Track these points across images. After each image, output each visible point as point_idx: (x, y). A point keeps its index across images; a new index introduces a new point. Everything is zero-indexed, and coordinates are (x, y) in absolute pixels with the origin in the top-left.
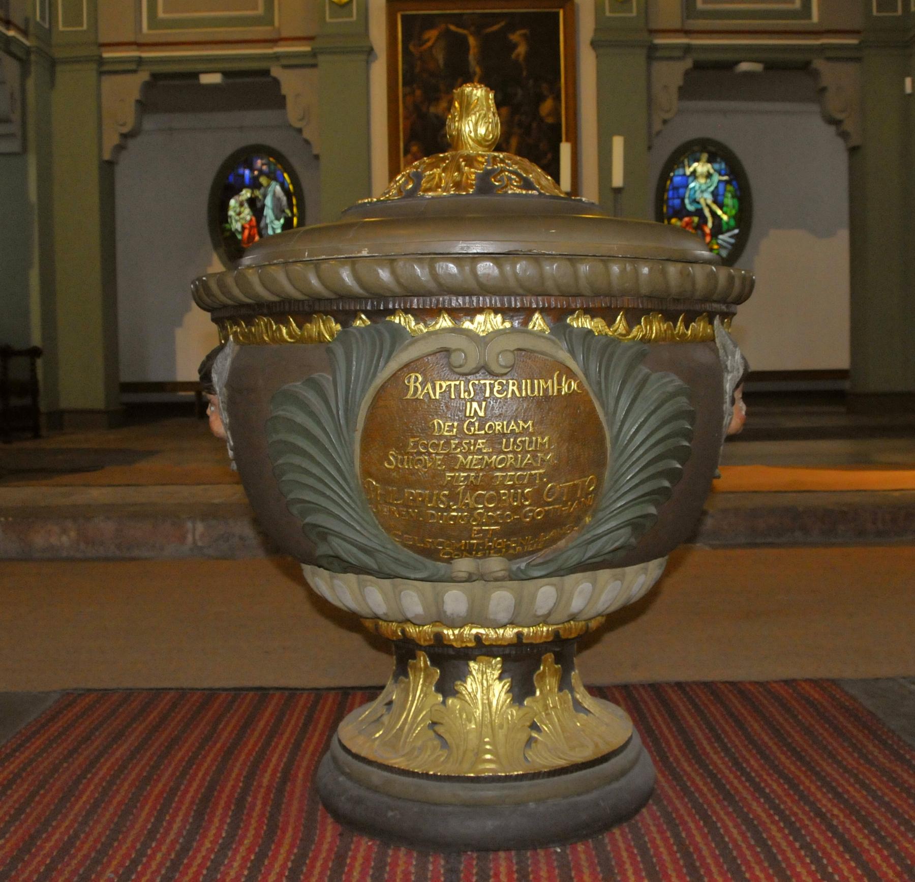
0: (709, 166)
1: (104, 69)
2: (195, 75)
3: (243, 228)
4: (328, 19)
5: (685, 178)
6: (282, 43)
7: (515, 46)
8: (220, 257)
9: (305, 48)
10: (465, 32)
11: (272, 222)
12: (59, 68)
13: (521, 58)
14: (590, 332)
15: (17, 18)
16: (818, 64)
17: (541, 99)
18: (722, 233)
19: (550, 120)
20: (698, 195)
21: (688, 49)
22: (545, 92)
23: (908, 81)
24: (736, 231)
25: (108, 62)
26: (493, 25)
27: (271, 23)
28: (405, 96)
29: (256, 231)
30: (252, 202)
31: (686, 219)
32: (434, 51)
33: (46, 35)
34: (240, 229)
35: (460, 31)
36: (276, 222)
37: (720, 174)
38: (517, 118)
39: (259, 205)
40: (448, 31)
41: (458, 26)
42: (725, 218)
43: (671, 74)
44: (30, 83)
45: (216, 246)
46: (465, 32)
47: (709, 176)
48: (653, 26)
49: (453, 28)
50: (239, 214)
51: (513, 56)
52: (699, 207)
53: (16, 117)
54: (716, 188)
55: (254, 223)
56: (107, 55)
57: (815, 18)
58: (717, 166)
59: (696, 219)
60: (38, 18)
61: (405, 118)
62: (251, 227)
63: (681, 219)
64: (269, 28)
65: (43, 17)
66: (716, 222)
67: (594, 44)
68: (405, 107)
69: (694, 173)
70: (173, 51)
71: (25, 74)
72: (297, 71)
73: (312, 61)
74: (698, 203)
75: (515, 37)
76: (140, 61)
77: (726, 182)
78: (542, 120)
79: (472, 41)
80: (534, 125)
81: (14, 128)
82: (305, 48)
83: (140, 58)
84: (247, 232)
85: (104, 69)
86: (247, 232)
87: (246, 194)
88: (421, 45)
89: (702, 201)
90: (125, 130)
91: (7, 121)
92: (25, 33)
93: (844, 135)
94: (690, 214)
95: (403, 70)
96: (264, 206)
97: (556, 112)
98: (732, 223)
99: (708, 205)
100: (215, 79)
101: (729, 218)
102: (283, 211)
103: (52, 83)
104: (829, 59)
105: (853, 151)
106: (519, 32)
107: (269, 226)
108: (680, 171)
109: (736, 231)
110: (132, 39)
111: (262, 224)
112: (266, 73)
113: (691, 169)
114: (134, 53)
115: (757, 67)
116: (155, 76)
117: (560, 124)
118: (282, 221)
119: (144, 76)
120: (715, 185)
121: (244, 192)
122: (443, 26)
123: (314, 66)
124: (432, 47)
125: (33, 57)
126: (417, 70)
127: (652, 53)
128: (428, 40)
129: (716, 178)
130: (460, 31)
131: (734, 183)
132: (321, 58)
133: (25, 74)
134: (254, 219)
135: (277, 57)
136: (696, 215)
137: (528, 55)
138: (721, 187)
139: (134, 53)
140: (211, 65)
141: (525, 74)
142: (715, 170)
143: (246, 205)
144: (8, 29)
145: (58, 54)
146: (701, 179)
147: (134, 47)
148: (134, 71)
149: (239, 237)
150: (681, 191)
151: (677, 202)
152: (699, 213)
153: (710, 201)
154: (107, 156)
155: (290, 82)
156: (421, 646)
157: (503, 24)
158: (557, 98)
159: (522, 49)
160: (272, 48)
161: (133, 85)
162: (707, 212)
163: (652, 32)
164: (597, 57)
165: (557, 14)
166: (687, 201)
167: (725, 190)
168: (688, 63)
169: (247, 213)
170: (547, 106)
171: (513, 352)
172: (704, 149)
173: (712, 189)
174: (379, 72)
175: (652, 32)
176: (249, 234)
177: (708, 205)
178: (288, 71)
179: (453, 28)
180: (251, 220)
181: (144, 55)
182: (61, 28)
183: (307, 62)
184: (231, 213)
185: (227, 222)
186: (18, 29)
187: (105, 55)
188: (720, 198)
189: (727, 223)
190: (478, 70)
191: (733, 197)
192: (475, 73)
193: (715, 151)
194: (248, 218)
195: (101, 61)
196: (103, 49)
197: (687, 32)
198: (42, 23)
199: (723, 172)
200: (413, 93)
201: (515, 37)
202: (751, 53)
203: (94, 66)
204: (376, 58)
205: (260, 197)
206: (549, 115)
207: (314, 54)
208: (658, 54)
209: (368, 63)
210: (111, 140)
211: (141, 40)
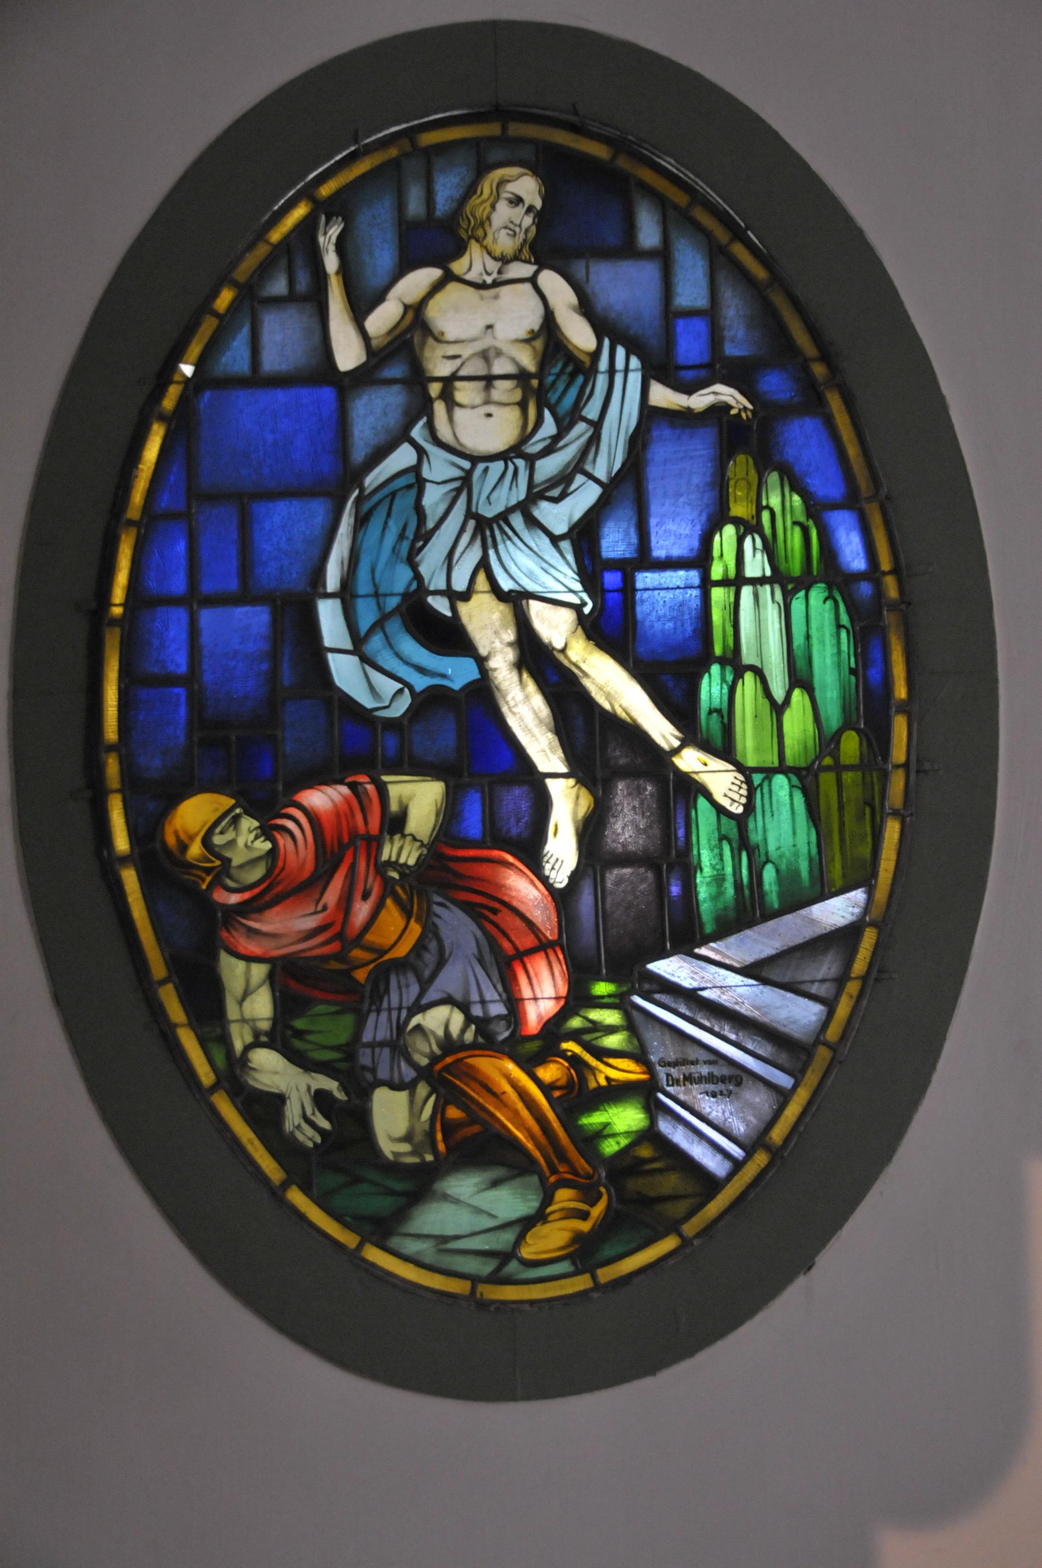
5: (328, 394)
14: (728, 407)
18: (686, 938)
37: (660, 368)
52: (458, 672)
58: (627, 287)
59: (421, 799)
63: (266, 805)
74: (450, 637)
89: (487, 624)
94: (362, 746)
98: (785, 827)
142: (602, 326)
150: (284, 523)
151: (240, 630)
152: (464, 735)
156: (865, 579)
162: (526, 714)
171: (526, 341)
172: (502, 130)
177: (535, 657)
199: (690, 345)
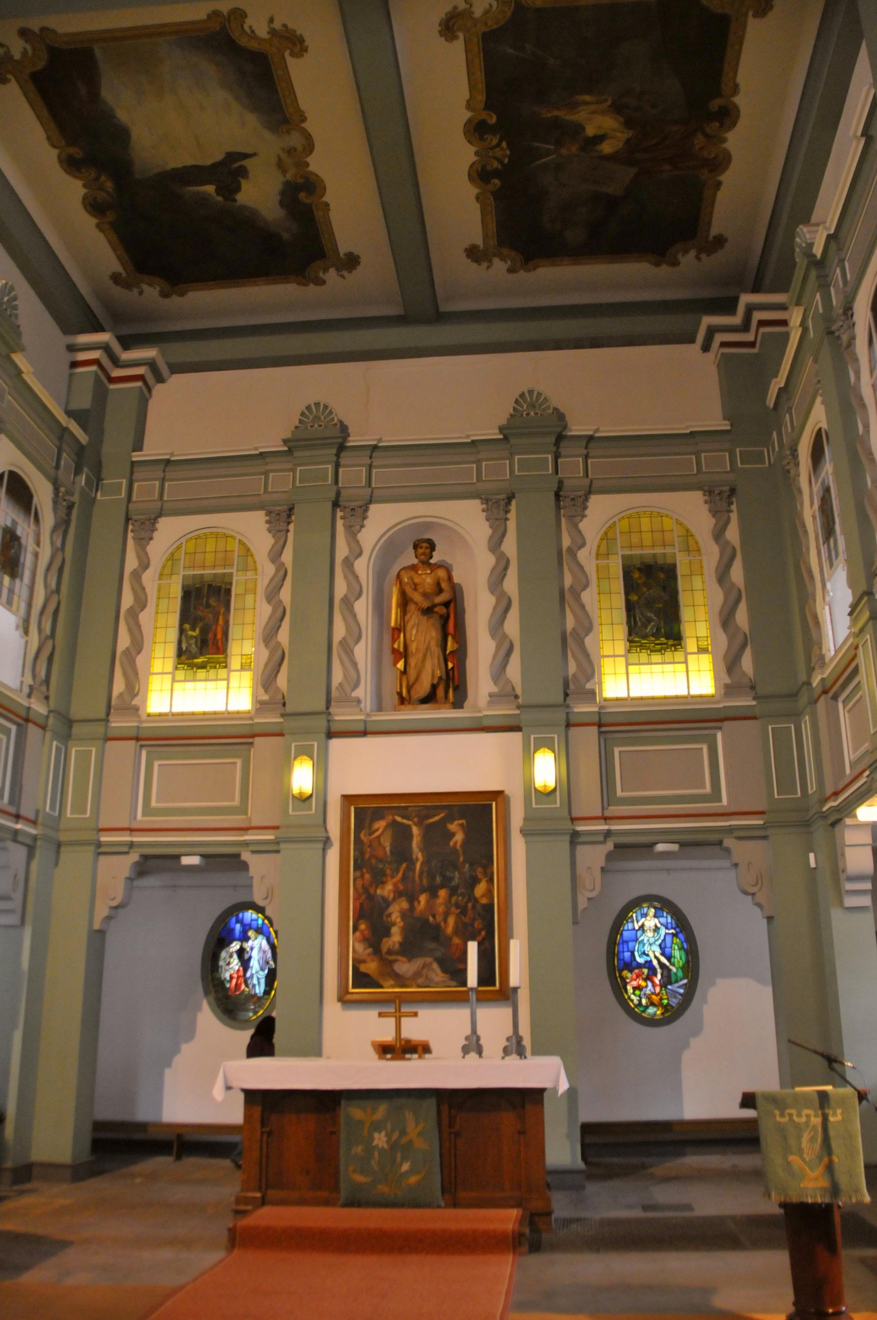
0: (656, 920)
1: (100, 850)
2: (177, 857)
3: (231, 977)
4: (291, 812)
6: (250, 832)
7: (453, 835)
8: (209, 1004)
9: (269, 836)
10: (410, 823)
11: (257, 972)
12: (63, 849)
13: (458, 845)
15: (26, 810)
16: (728, 842)
17: (475, 881)
18: (671, 984)
19: (484, 901)
20: (647, 948)
21: (608, 834)
22: (480, 876)
23: (812, 856)
24: (685, 981)
25: (105, 845)
26: (435, 816)
27: (246, 813)
28: (355, 880)
29: (242, 980)
30: (241, 952)
31: (636, 971)
32: (382, 839)
33: (55, 823)
34: (228, 978)
35: (405, 821)
36: (261, 973)
37: (667, 928)
38: (454, 899)
39: (246, 956)
40: (394, 822)
41: (403, 817)
42: (674, 969)
43: (593, 857)
44: (34, 865)
45: (207, 993)
46: (410, 823)
47: (656, 929)
48: (574, 815)
49: (398, 819)
50: (229, 964)
51: (451, 844)
52: (648, 959)
53: (18, 896)
54: (664, 940)
55: (241, 973)
56: (105, 838)
57: (725, 801)
58: (663, 920)
60: (48, 809)
61: (355, 899)
62: (238, 977)
64: (245, 817)
65: (53, 807)
66: (665, 973)
67: (524, 832)
68: (355, 889)
69: (642, 927)
70: (158, 836)
71: (31, 856)
72: (264, 856)
73: (275, 848)
74: (648, 955)
75: (453, 827)
76: (131, 845)
77: (673, 935)
78: (476, 900)
79: (415, 830)
80: (470, 905)
81: (16, 904)
82: (269, 836)
83: (132, 842)
84: (234, 981)
85: (100, 850)
86: (234, 981)
87: (235, 946)
88: (370, 835)
90: (114, 903)
91: (8, 898)
92: (34, 823)
93: (759, 905)
94: (640, 966)
95: (354, 856)
96: (250, 958)
97: (489, 893)
98: (680, 974)
99: (656, 957)
100: (195, 860)
101: (677, 969)
102: (268, 963)
103: (57, 863)
104: (739, 838)
105: (770, 919)
106: (456, 822)
107: (255, 976)
108: (630, 926)
109: (685, 981)
110: (127, 825)
111: (248, 974)
112: (238, 856)
113: (640, 924)
114: (126, 838)
115: (675, 847)
116: (145, 858)
117: (493, 905)
118: (266, 971)
119: (134, 857)
120: (662, 938)
121: (234, 944)
122: (390, 817)
123: (278, 851)
124: (380, 835)
125: (39, 843)
126: (367, 856)
127: (575, 838)
128: (377, 830)
129: (663, 931)
130: (405, 821)
131: (681, 935)
132: (283, 846)
133: (31, 856)
134: (241, 969)
135: (246, 844)
136: (645, 967)
137: (465, 843)
138: (668, 939)
139: (126, 838)
140: (191, 848)
141: (461, 859)
142: (661, 924)
143: (235, 956)
144: (17, 823)
145: (63, 837)
146: (650, 935)
147: (128, 832)
148: (127, 853)
149: (228, 985)
150: (631, 944)
153: (658, 954)
154: (97, 926)
155: (257, 865)
157: (442, 815)
158: (491, 880)
159: (459, 837)
160: (242, 835)
161: (126, 863)
162: (655, 962)
163: (573, 820)
164: (526, 842)
165: (491, 805)
166: (636, 954)
167: (673, 943)
168: (610, 846)
169: (235, 963)
170: (480, 889)
173: (660, 941)
174: (333, 856)
175: (573, 820)
176: (236, 984)
177: (656, 957)
178: (256, 856)
179: (398, 819)
180: (238, 970)
181: (135, 839)
182: (69, 815)
183: (271, 849)
184: (221, 963)
185: (217, 971)
186: (27, 820)
187: (103, 839)
188: (667, 950)
189: (676, 974)
190: (420, 855)
191: (679, 949)
192: (417, 859)
193: (664, 905)
194: (237, 968)
195: (99, 844)
196: (101, 833)
197: (606, 819)
198: (52, 813)
199: (669, 926)
200: (362, 876)
201: (453, 827)
202: (666, 835)
203: (92, 848)
204: (331, 845)
205: (248, 949)
206: (483, 896)
207: (277, 842)
208: (581, 840)
209: (324, 850)
210: (102, 911)
211: (135, 825)
